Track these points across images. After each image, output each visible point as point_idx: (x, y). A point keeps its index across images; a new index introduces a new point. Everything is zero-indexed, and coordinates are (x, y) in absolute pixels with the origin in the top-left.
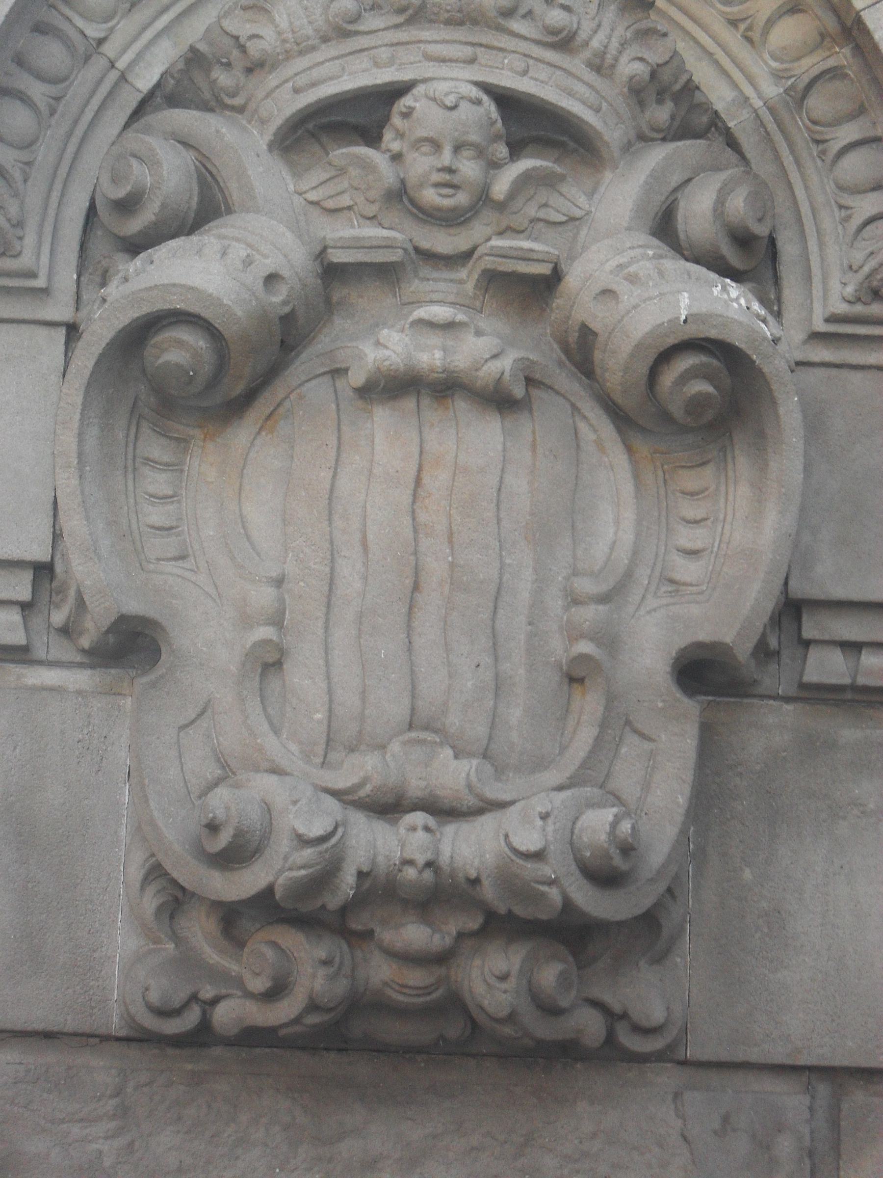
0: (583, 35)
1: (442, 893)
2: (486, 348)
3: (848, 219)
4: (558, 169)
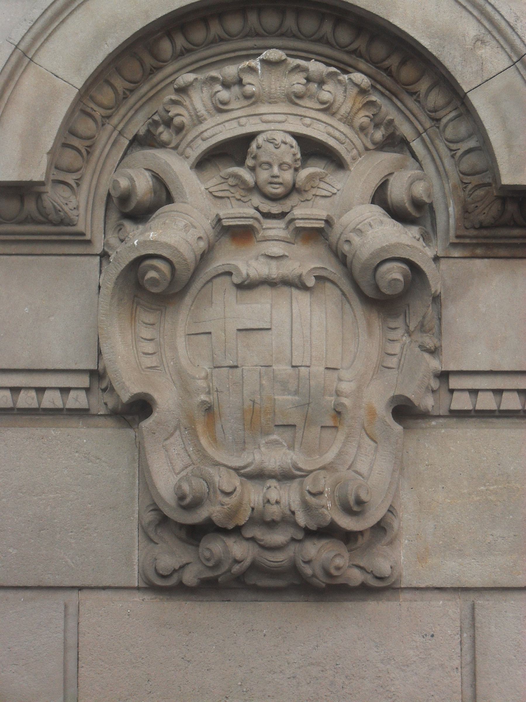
0: (336, 105)
2: (305, 261)
4: (326, 172)
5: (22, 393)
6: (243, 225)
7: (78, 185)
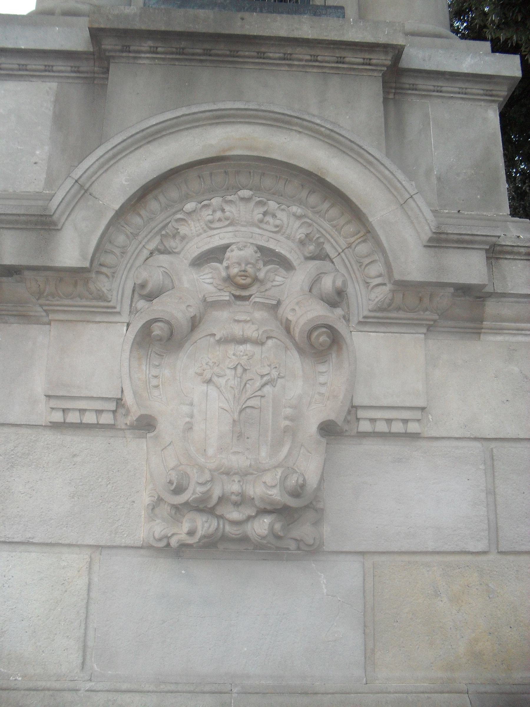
1: (242, 500)
3: (369, 286)
5: (87, 413)
6: (247, 156)
7: (113, 277)
